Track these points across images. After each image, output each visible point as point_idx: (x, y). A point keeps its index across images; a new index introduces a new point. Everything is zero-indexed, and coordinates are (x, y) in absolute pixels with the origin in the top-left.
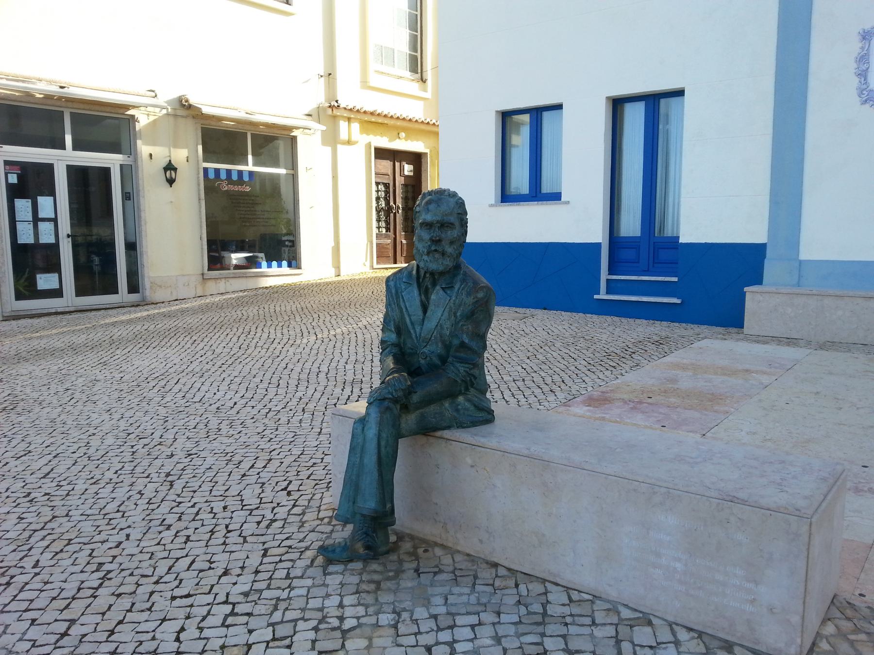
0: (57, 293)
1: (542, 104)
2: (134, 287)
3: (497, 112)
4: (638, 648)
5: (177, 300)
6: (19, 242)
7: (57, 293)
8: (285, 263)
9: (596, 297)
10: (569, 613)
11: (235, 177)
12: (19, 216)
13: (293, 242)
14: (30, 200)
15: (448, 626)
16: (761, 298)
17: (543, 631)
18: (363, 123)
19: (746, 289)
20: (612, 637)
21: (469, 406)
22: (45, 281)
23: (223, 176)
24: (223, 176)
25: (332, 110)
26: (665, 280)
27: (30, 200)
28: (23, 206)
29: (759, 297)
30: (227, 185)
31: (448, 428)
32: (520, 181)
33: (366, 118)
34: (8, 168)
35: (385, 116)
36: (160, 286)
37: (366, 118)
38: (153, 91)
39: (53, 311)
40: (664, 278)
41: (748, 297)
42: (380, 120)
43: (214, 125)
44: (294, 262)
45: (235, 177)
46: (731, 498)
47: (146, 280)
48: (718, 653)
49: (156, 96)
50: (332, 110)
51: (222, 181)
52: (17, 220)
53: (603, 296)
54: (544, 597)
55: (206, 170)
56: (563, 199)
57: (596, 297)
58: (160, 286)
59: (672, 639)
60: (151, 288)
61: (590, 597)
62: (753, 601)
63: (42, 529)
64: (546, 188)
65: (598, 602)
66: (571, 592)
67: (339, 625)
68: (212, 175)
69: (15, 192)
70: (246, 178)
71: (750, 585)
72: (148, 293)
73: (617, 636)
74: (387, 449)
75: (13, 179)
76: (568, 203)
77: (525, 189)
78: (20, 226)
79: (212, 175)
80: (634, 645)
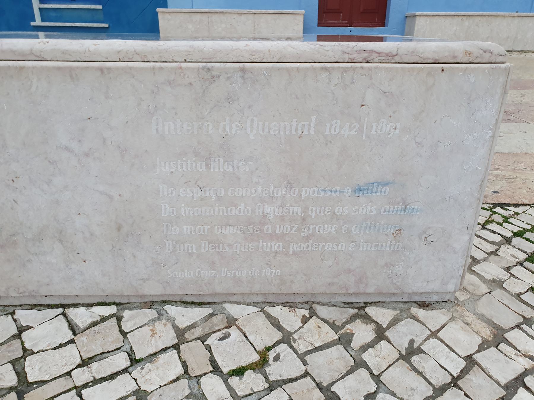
4: (234, 381)
9: (32, 24)
10: (78, 361)
15: (185, 362)
16: (170, 17)
17: (137, 387)
20: (178, 379)
29: (167, 16)
41: (160, 17)
46: (366, 55)
48: (353, 329)
53: (38, 22)
54: (17, 343)
59: (278, 336)
61: (112, 310)
65: (126, 314)
66: (70, 312)
67: (373, 325)
73: (186, 372)
80: (225, 377)
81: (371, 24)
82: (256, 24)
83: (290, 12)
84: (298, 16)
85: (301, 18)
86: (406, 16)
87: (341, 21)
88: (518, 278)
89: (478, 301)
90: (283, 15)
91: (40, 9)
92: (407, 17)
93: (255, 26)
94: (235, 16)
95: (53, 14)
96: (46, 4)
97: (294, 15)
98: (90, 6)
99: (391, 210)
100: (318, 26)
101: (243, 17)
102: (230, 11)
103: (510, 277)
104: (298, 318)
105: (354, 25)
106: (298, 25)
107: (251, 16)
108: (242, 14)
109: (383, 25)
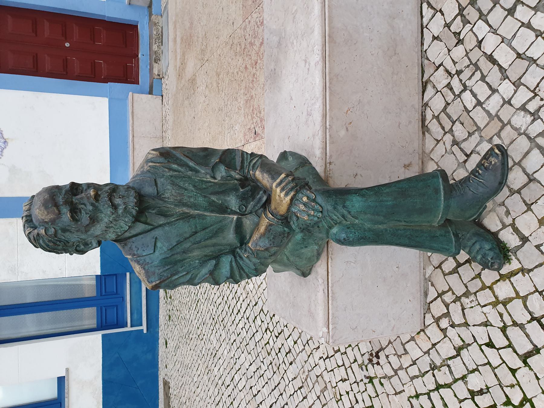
9: (145, 332)
81: (136, 38)
82: (143, 136)
83: (131, 105)
84: (135, 98)
85: (136, 96)
86: (129, 4)
87: (134, 65)
88: (481, 374)
89: (514, 90)
90: (134, 111)
91: (131, 327)
92: (131, 3)
93: (144, 137)
94: (135, 153)
95: (135, 316)
96: (127, 322)
97: (134, 101)
98: (127, 284)
99: (178, 277)
100: (139, 84)
101: (137, 146)
102: (131, 158)
103: (342, 395)
104: (417, 55)
105: (137, 53)
106: (142, 99)
107: (135, 139)
108: (134, 147)
109: (136, 27)
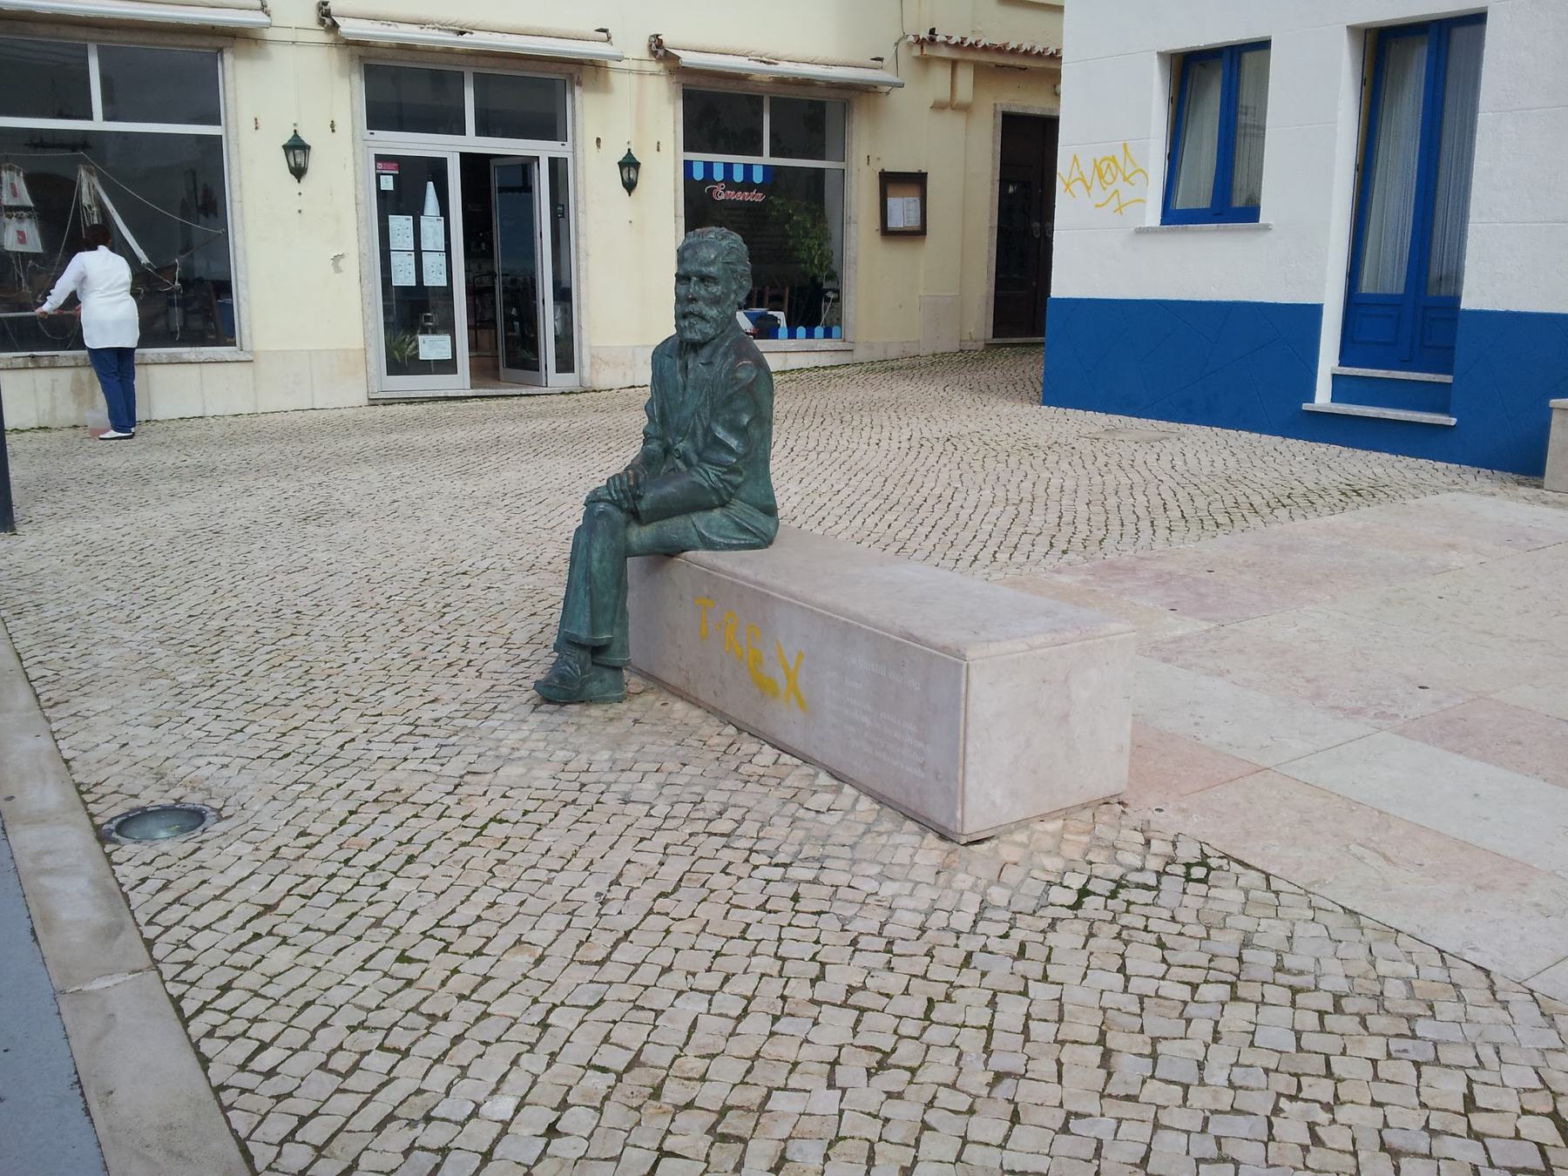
0: (448, 367)
1: (1219, 41)
2: (566, 363)
3: (1160, 54)
5: (633, 387)
6: (1401, 291)
7: (448, 367)
8: (819, 330)
11: (738, 176)
12: (394, 244)
13: (837, 291)
14: (411, 217)
18: (980, 70)
19: (1554, 402)
21: (727, 523)
22: (432, 347)
23: (718, 174)
24: (718, 174)
25: (922, 48)
26: (1436, 380)
27: (411, 217)
28: (400, 225)
30: (724, 191)
31: (695, 548)
32: (1198, 189)
33: (984, 58)
34: (380, 165)
35: (1027, 53)
36: (607, 363)
37: (984, 58)
38: (605, 31)
39: (442, 394)
40: (1433, 375)
42: (1011, 61)
43: (705, 85)
44: (835, 330)
45: (738, 176)
47: (585, 351)
49: (609, 38)
50: (922, 48)
51: (717, 183)
52: (392, 248)
55: (688, 165)
56: (1262, 220)
57: (1306, 406)
58: (607, 363)
60: (592, 364)
62: (922, 765)
63: (273, 644)
64: (1239, 201)
68: (698, 174)
69: (389, 204)
70: (758, 177)
71: (920, 745)
72: (586, 373)
74: (604, 564)
75: (388, 184)
76: (1267, 228)
77: (1204, 202)
78: (395, 259)
79: (698, 174)
